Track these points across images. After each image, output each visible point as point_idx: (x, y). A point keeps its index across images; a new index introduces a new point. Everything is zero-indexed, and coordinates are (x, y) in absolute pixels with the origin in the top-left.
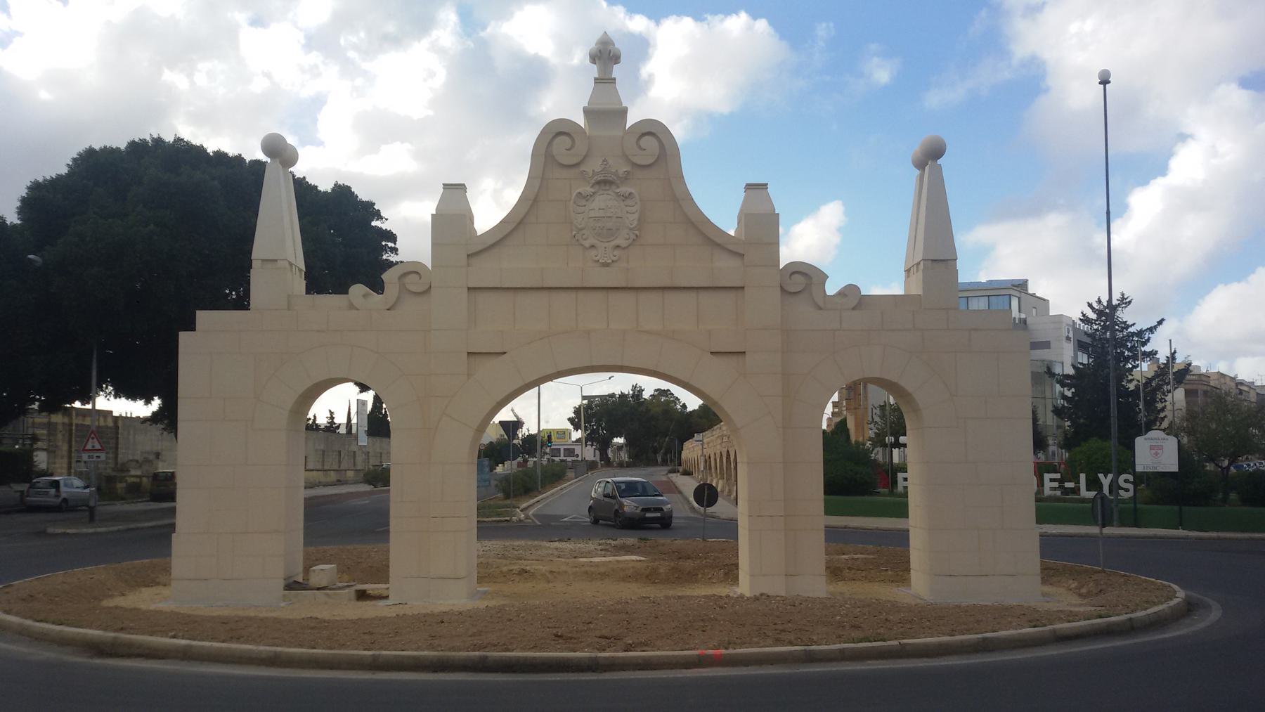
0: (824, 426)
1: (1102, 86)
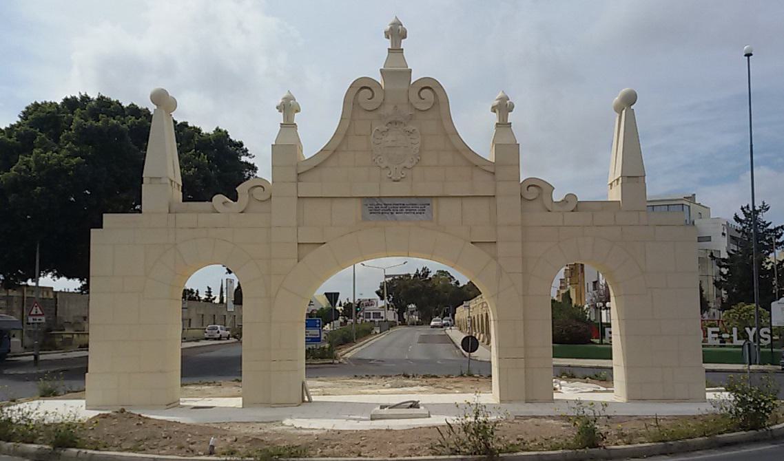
0: (554, 295)
1: (747, 58)
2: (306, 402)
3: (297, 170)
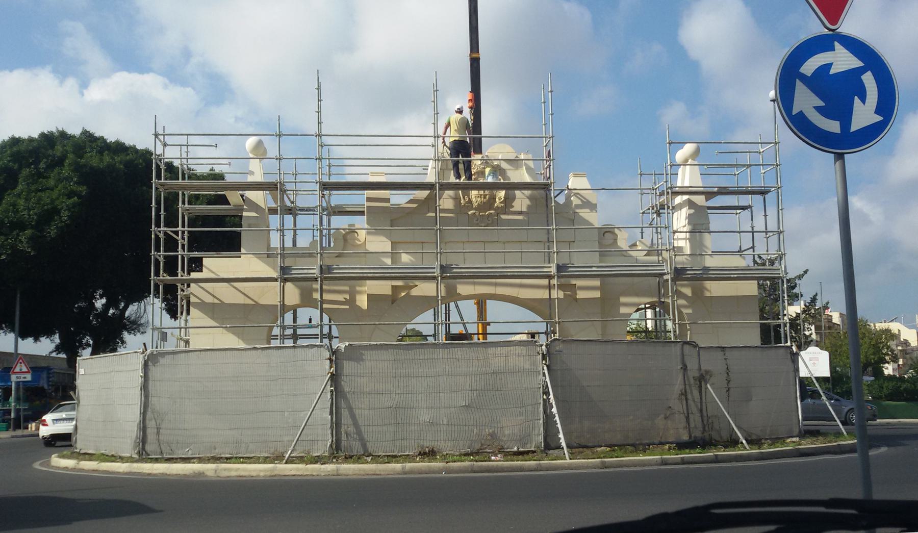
3: (206, 268)
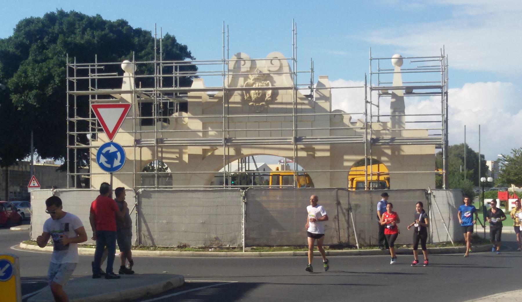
2: (103, 274)
3: (100, 138)
